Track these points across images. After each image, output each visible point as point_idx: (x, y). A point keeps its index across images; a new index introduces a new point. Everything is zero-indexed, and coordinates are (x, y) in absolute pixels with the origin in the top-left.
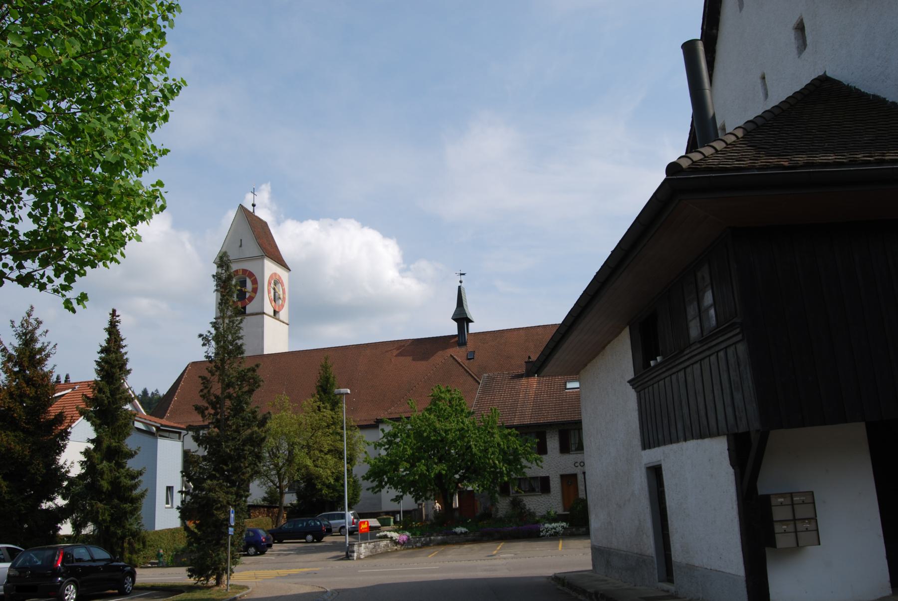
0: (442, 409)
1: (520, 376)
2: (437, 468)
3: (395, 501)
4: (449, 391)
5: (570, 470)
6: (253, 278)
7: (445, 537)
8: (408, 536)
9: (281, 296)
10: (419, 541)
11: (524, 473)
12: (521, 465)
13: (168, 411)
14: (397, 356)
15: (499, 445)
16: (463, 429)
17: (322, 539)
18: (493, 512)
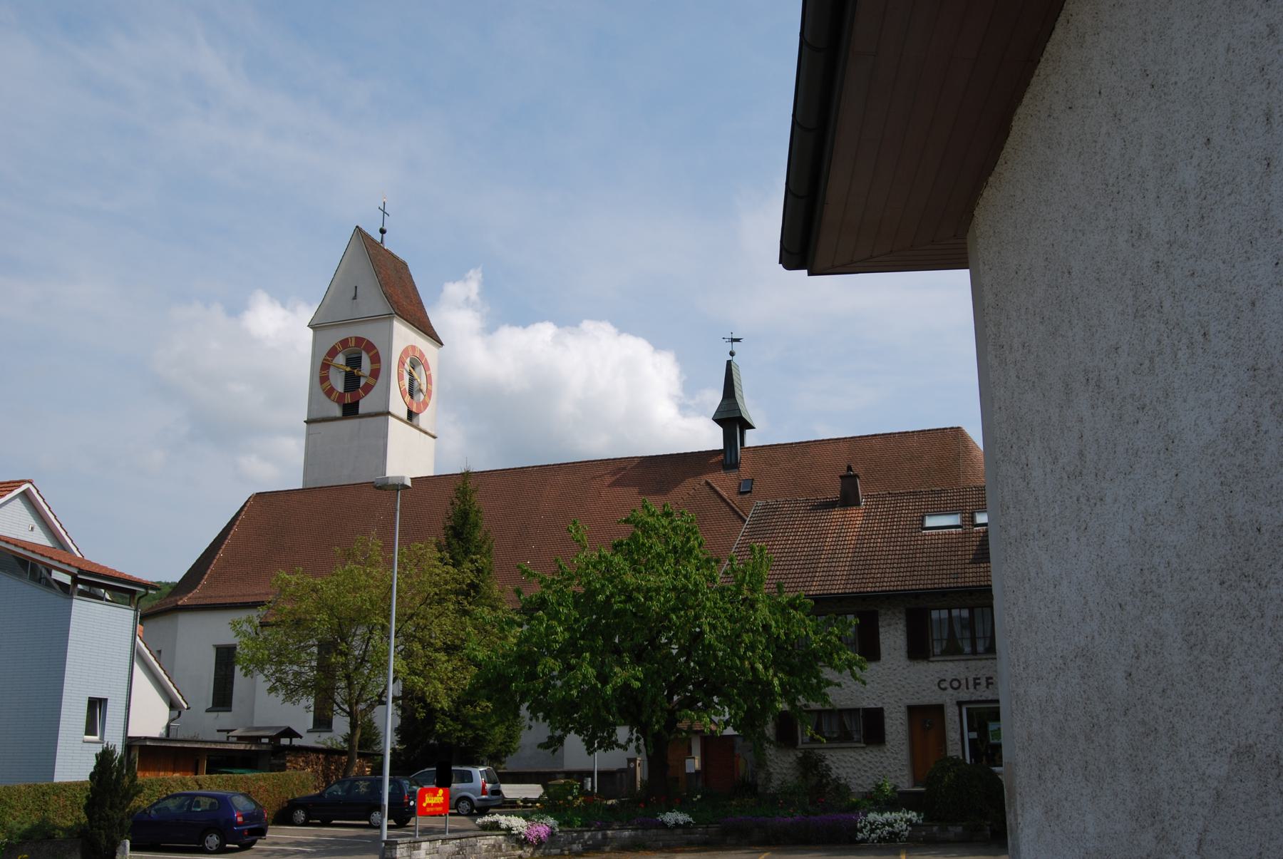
0: (643, 544)
1: (829, 505)
2: (620, 675)
3: (546, 748)
4: (667, 515)
5: (930, 696)
6: (372, 353)
7: (640, 832)
8: (552, 828)
9: (424, 387)
10: (578, 838)
11: (825, 694)
12: (817, 677)
13: (206, 577)
15: (766, 627)
16: (685, 588)
17: (408, 820)
18: (759, 782)
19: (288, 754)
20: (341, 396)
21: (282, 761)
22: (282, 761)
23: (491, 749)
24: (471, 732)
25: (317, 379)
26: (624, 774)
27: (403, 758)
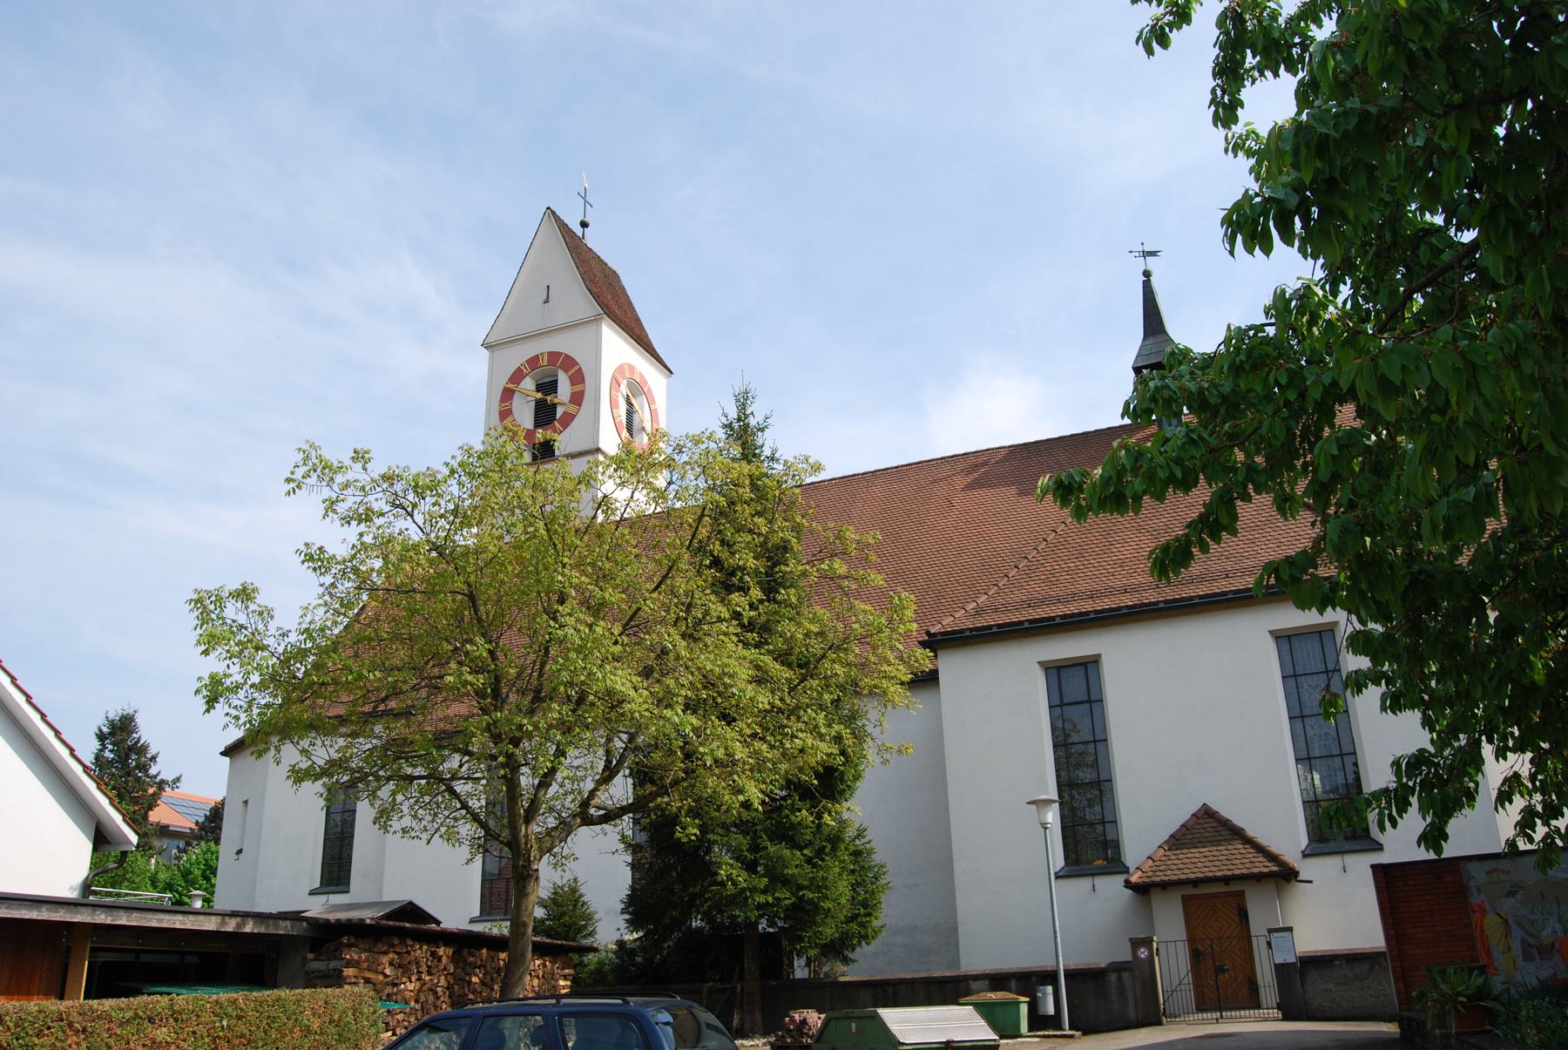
14: (966, 488)
19: (350, 946)
20: (530, 435)
21: (333, 965)
22: (333, 965)
23: (829, 932)
24: (788, 895)
25: (496, 416)
26: (1125, 975)
27: (639, 959)
